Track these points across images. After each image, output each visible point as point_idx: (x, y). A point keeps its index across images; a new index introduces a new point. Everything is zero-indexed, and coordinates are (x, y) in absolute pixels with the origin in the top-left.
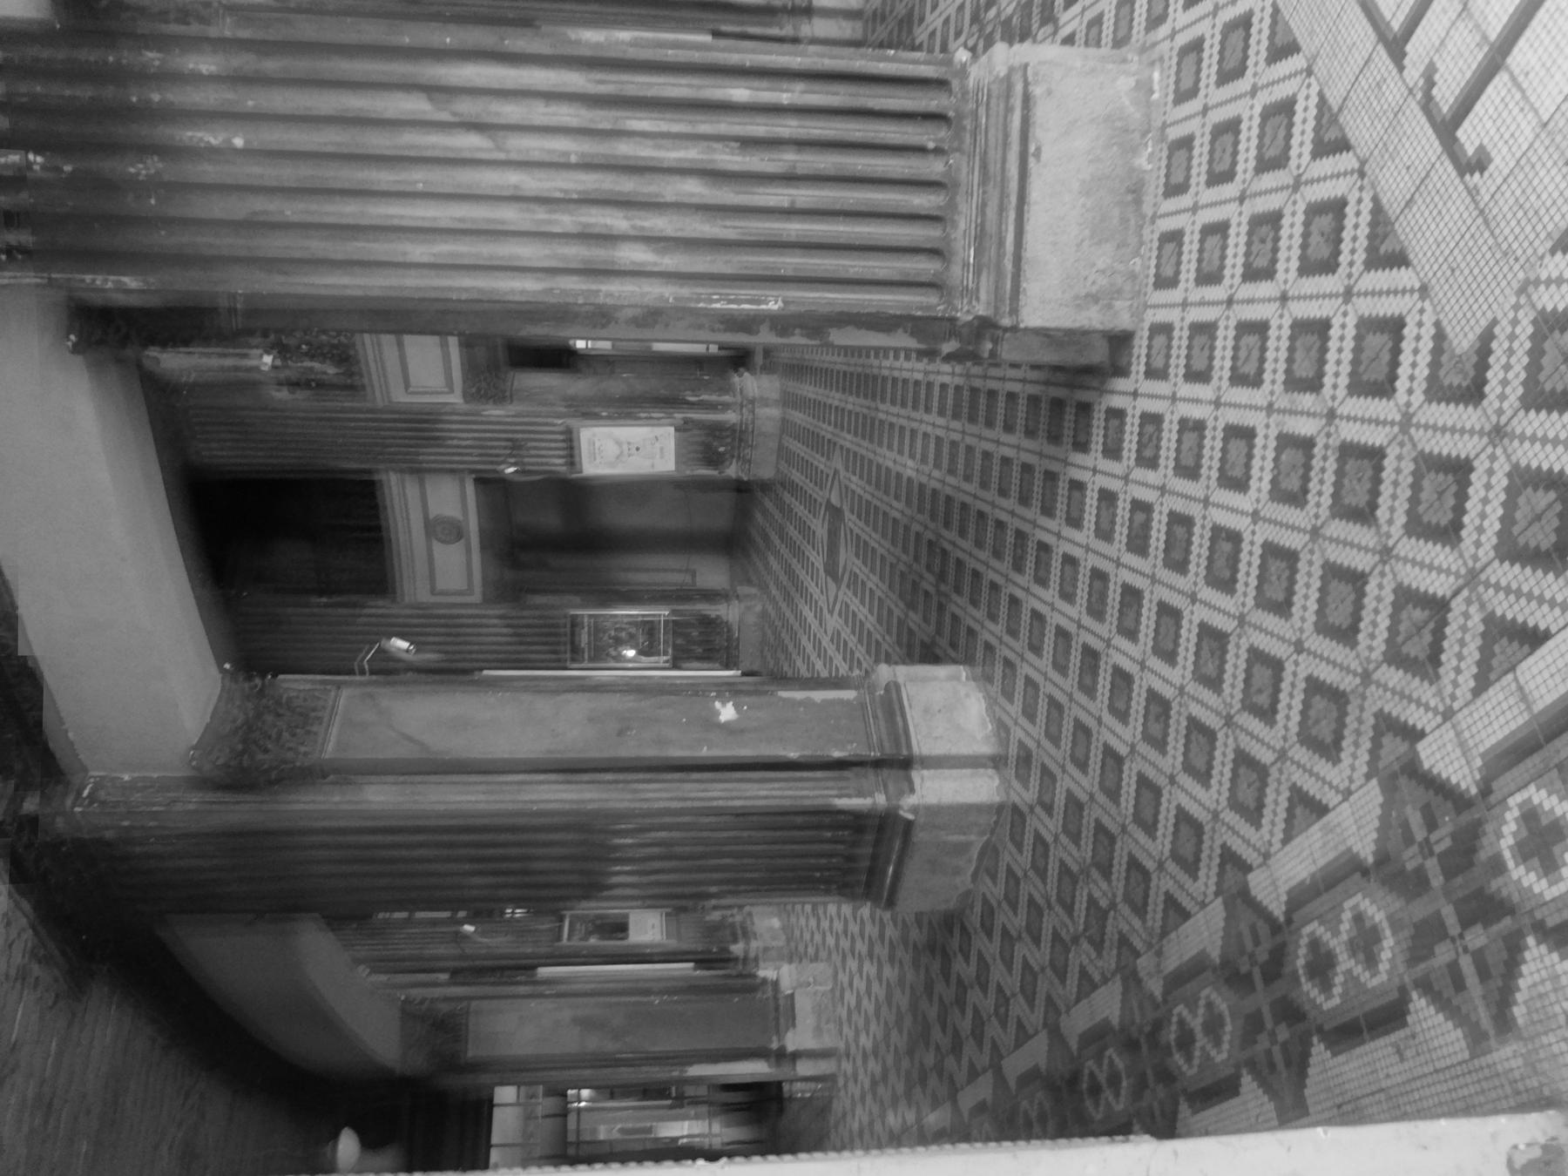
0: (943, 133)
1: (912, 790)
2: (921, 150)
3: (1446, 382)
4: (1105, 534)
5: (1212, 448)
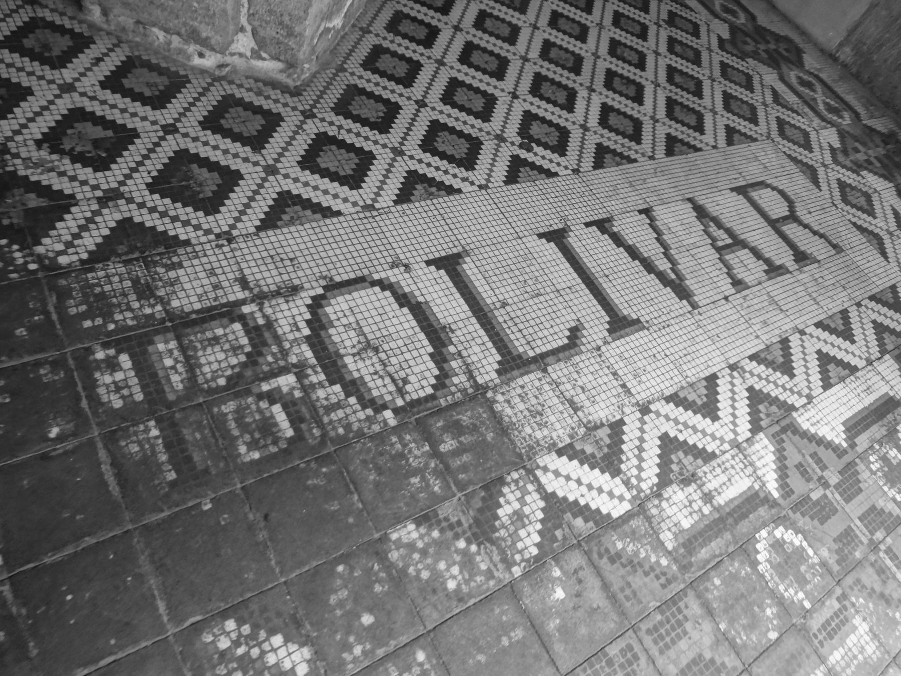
3: (418, 187)
5: (426, 15)
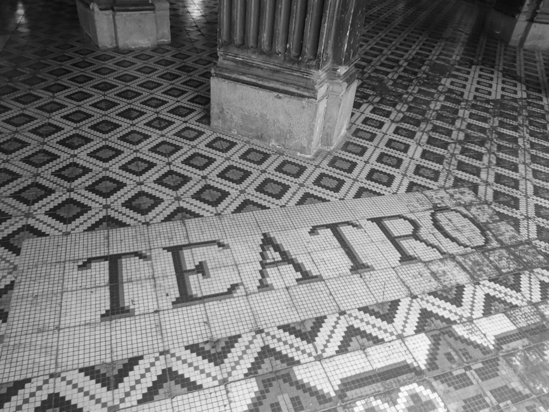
0: (293, 53)
1: (101, 9)
2: (287, 41)
4: (390, 143)
